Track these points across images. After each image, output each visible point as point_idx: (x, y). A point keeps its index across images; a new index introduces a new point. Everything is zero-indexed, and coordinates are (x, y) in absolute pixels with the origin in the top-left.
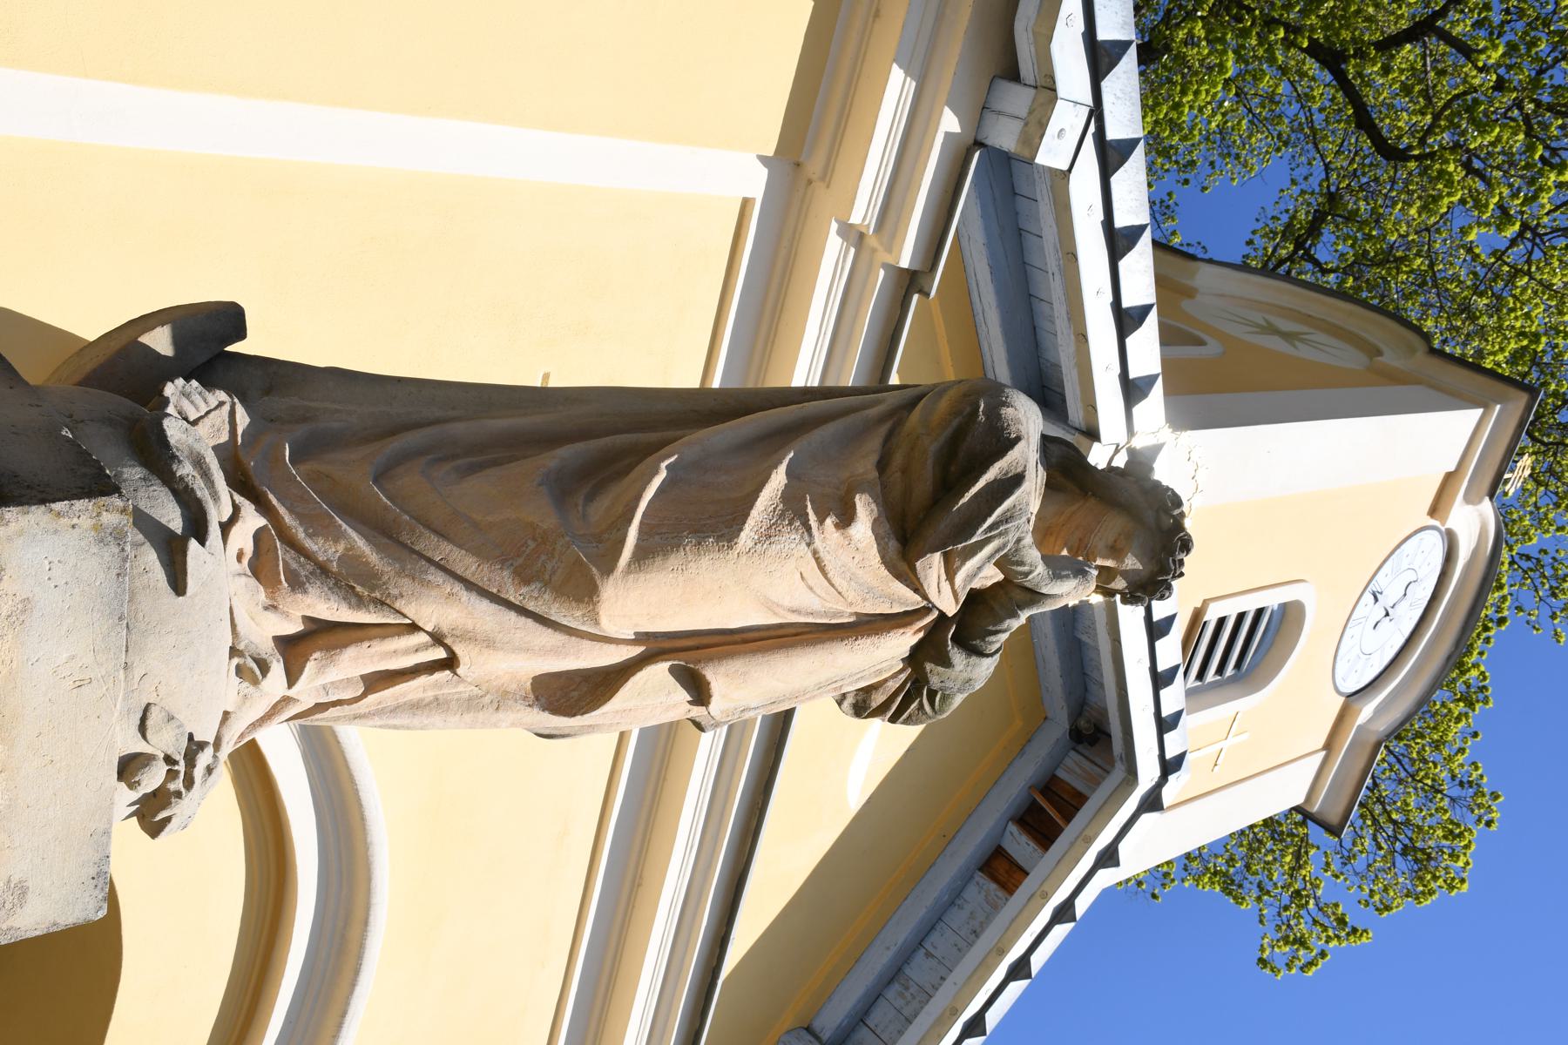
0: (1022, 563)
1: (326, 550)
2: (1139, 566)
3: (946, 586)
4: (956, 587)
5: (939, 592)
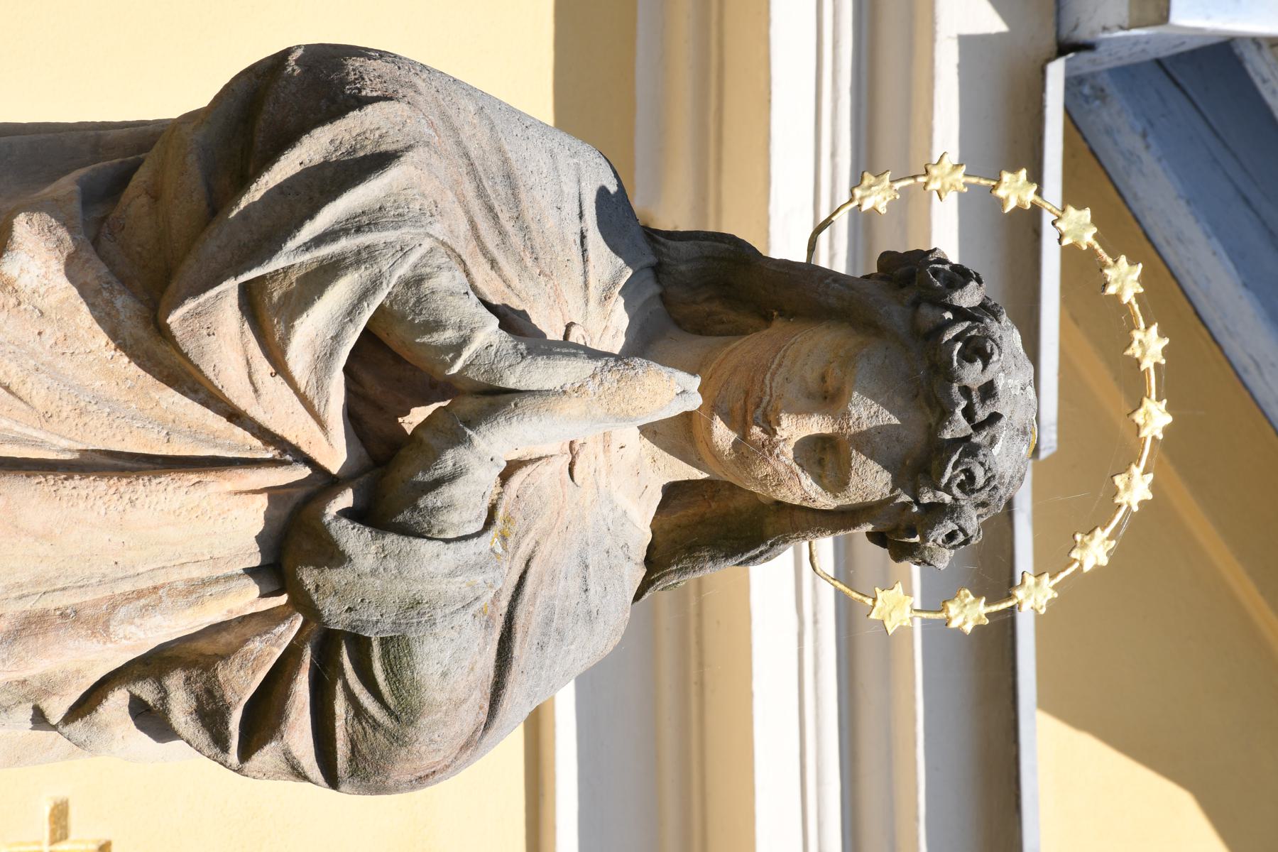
0: (437, 326)
2: (888, 418)
3: (274, 386)
4: (302, 385)
5: (256, 391)
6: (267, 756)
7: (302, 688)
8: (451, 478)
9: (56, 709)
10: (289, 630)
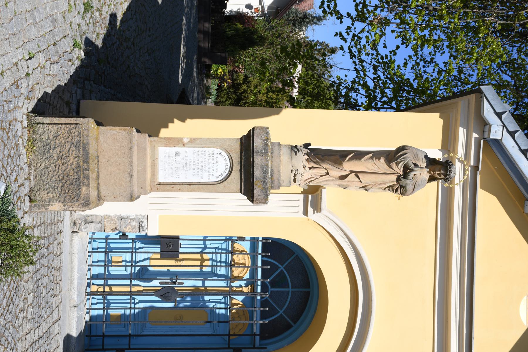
1: (314, 160)
2: (444, 172)
6: (397, 193)
7: (399, 189)
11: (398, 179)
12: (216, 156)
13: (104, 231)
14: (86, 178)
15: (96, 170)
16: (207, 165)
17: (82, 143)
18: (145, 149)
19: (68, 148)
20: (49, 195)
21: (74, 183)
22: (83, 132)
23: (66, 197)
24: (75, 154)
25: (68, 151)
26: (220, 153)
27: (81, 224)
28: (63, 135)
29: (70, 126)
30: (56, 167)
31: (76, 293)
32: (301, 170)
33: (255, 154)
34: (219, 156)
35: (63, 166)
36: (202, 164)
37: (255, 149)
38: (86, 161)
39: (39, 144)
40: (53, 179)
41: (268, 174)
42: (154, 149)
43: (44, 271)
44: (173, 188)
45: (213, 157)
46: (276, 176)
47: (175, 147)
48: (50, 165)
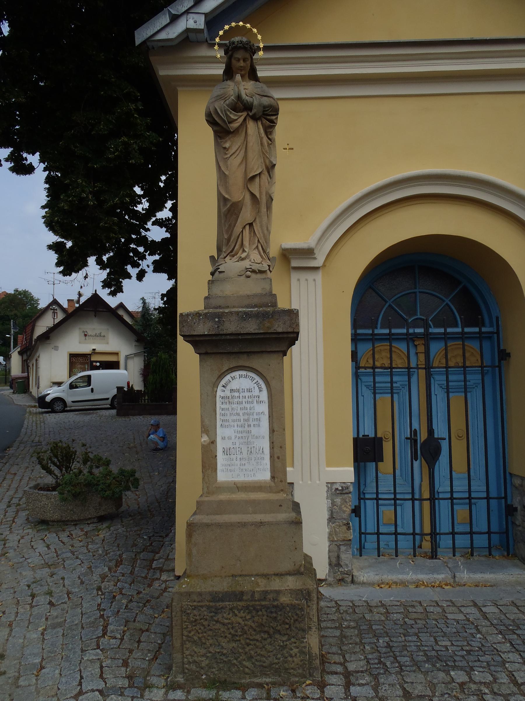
3: (238, 120)
6: (275, 121)
7: (269, 117)
8: (247, 101)
9: (270, 142)
10: (263, 119)
11: (255, 118)
12: (228, 393)
13: (350, 540)
14: (266, 596)
15: (253, 579)
16: (242, 406)
17: (211, 604)
18: (221, 502)
19: (218, 626)
20: (294, 655)
21: (274, 615)
22: (195, 601)
23: (296, 628)
24: (229, 614)
25: (224, 625)
26: (224, 386)
27: (341, 571)
28: (199, 633)
29: (186, 622)
30: (250, 644)
31: (435, 576)
32: (246, 264)
33: (222, 332)
34: (229, 387)
35: (248, 632)
36: (241, 414)
37: (213, 333)
38: (239, 596)
39: (214, 670)
40: (269, 647)
41: (252, 311)
42: (220, 487)
43: (412, 644)
44: (278, 458)
45: (230, 397)
46: (256, 301)
47: (216, 456)
48: (246, 653)
